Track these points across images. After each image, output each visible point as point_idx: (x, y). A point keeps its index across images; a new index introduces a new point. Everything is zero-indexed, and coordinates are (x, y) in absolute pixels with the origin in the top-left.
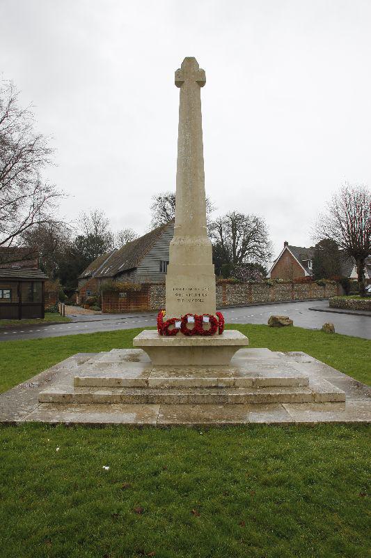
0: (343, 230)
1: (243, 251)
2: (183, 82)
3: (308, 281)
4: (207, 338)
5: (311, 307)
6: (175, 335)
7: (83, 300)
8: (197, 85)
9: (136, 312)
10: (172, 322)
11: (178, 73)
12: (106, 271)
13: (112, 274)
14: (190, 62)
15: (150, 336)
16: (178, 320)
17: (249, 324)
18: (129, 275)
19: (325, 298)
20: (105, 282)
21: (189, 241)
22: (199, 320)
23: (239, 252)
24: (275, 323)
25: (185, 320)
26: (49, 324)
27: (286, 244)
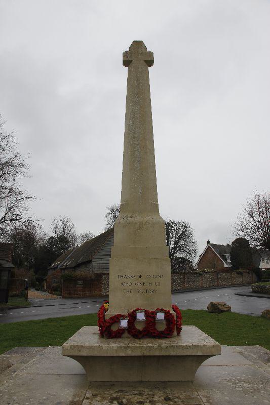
0: (258, 227)
1: (175, 248)
2: (131, 62)
3: (226, 270)
4: (165, 343)
5: (236, 292)
6: (120, 337)
7: (49, 287)
8: (145, 64)
9: (90, 297)
10: (117, 319)
11: (125, 54)
12: (67, 263)
13: (73, 265)
14: (138, 45)
15: (88, 338)
16: (123, 317)
17: (189, 309)
18: (86, 267)
19: (249, 284)
20: (66, 272)
21: (138, 218)
22: (151, 316)
23: (172, 249)
24: (215, 309)
25: (132, 317)
26: (10, 309)
27: (208, 242)
